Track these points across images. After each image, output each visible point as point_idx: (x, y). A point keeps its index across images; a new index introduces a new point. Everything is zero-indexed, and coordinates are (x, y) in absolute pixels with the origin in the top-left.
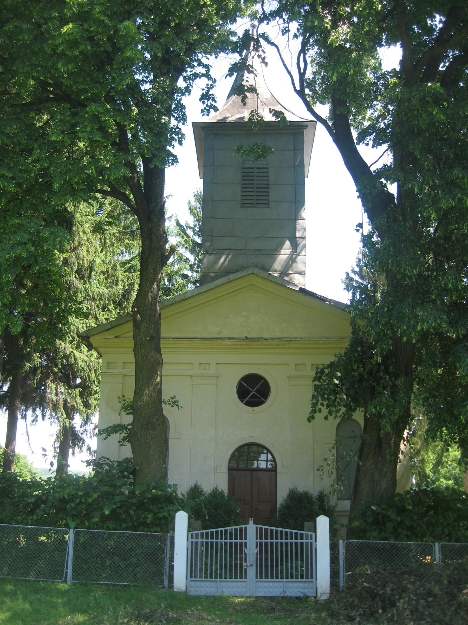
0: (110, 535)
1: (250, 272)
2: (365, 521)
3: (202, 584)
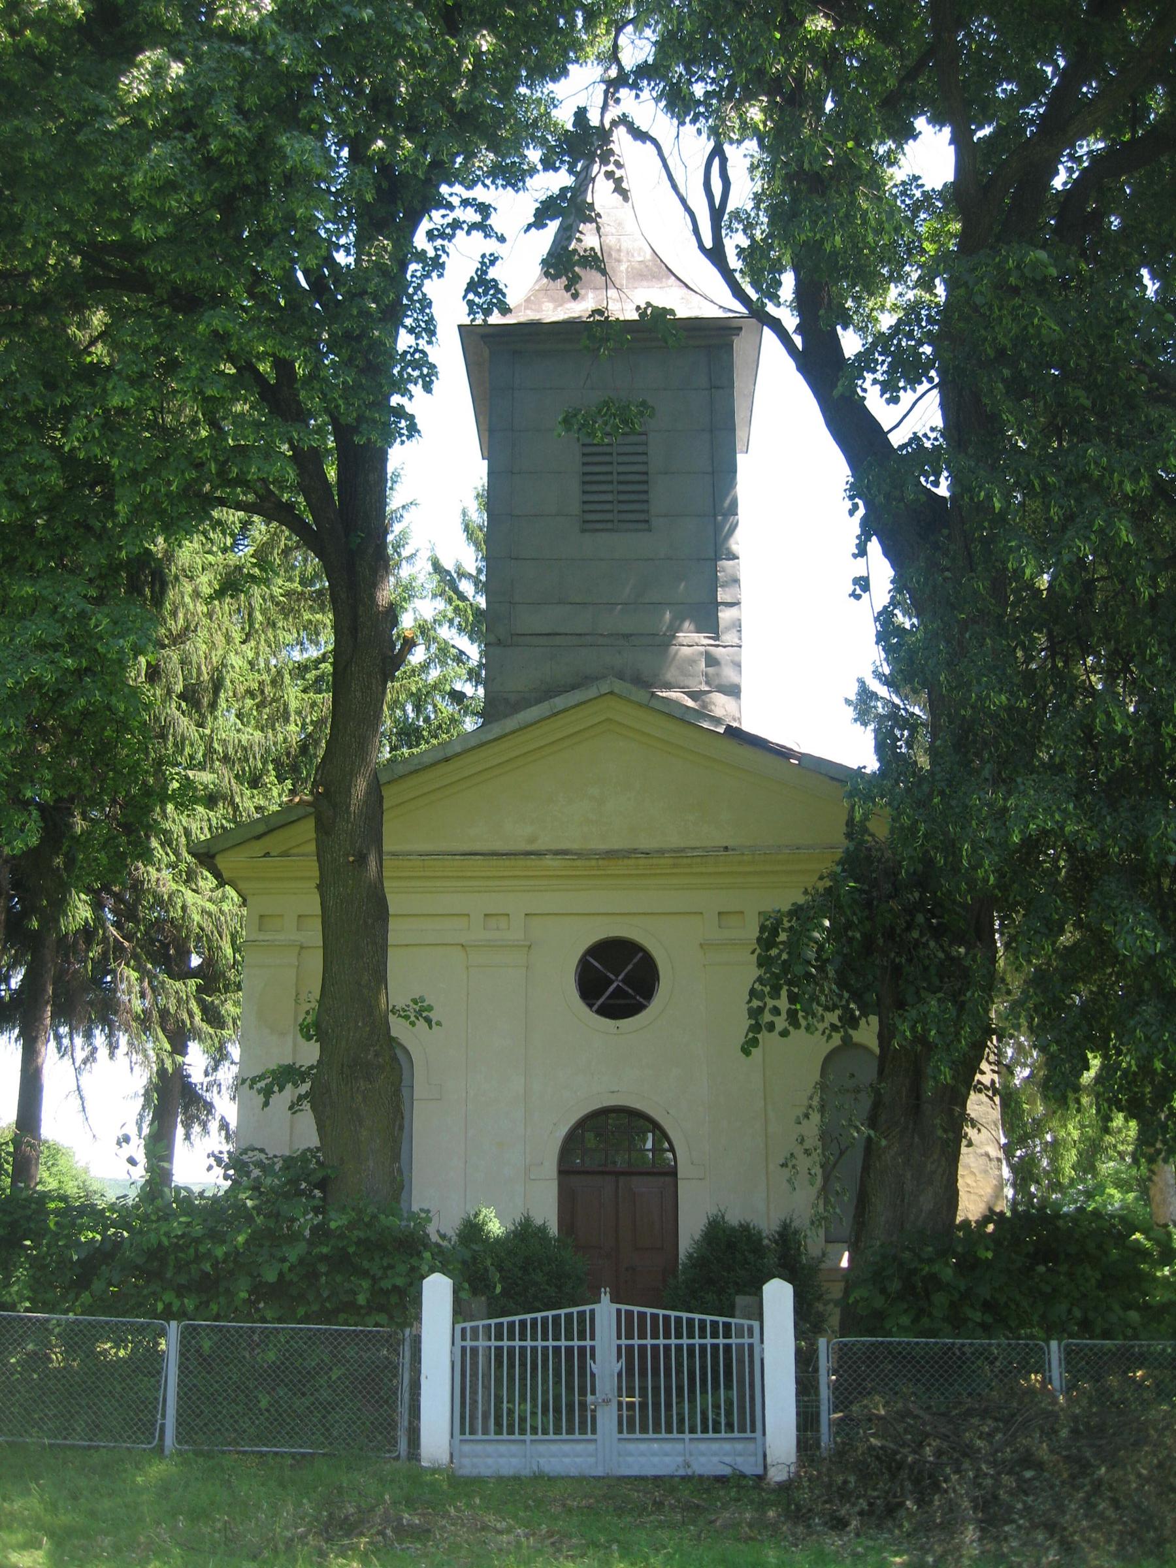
0: (266, 1334)
1: (605, 689)
2: (883, 1291)
3: (490, 1448)
